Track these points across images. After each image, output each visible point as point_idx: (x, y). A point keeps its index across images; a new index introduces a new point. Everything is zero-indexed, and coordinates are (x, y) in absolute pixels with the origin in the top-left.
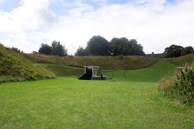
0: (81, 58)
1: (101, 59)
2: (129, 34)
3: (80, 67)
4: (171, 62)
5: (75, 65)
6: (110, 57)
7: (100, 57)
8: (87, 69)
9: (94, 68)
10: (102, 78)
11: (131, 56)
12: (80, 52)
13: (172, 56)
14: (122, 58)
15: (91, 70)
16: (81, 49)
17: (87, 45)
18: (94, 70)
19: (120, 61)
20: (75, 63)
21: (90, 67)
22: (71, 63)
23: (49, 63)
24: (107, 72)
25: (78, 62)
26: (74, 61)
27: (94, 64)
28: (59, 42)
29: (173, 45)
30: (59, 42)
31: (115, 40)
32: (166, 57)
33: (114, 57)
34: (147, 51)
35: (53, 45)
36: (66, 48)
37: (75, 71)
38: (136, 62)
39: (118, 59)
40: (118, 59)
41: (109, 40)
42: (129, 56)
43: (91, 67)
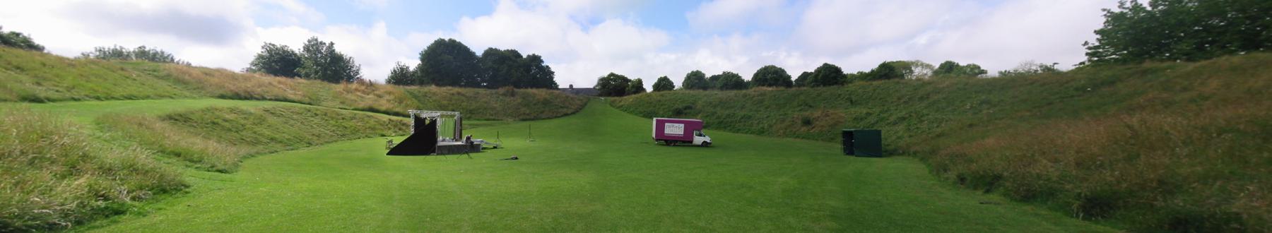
0: (401, 89)
1: (459, 93)
2: (167, 51)
3: (397, 114)
4: (612, 104)
5: (383, 108)
6: (481, 91)
7: (456, 90)
8: (419, 121)
9: (442, 116)
10: (471, 148)
11: (534, 91)
12: (400, 77)
13: (609, 94)
14: (513, 95)
15: (433, 122)
16: (402, 69)
17: (1071, 68)
18: (444, 124)
19: (508, 99)
20: (384, 104)
21: (426, 115)
22: (369, 100)
23: (246, 98)
24: (477, 125)
25: (389, 101)
26: (380, 96)
27: (442, 108)
28: (332, 44)
29: (612, 74)
30: (332, 44)
31: (491, 53)
32: (601, 95)
33: (480, 87)
34: (563, 79)
35: (307, 48)
36: (357, 64)
37: (383, 124)
38: (546, 102)
39: (504, 95)
40: (504, 95)
41: (479, 52)
42: (530, 90)
43: (435, 114)
